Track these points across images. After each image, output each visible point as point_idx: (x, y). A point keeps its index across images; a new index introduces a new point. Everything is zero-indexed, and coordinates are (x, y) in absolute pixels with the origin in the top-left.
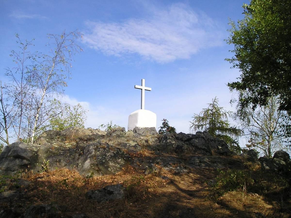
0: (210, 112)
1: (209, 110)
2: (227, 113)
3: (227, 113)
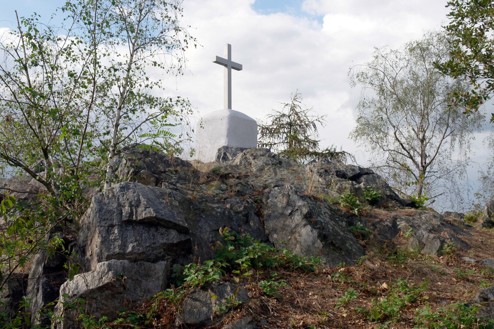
0: (285, 120)
1: (284, 115)
2: (316, 120)
3: (316, 122)
